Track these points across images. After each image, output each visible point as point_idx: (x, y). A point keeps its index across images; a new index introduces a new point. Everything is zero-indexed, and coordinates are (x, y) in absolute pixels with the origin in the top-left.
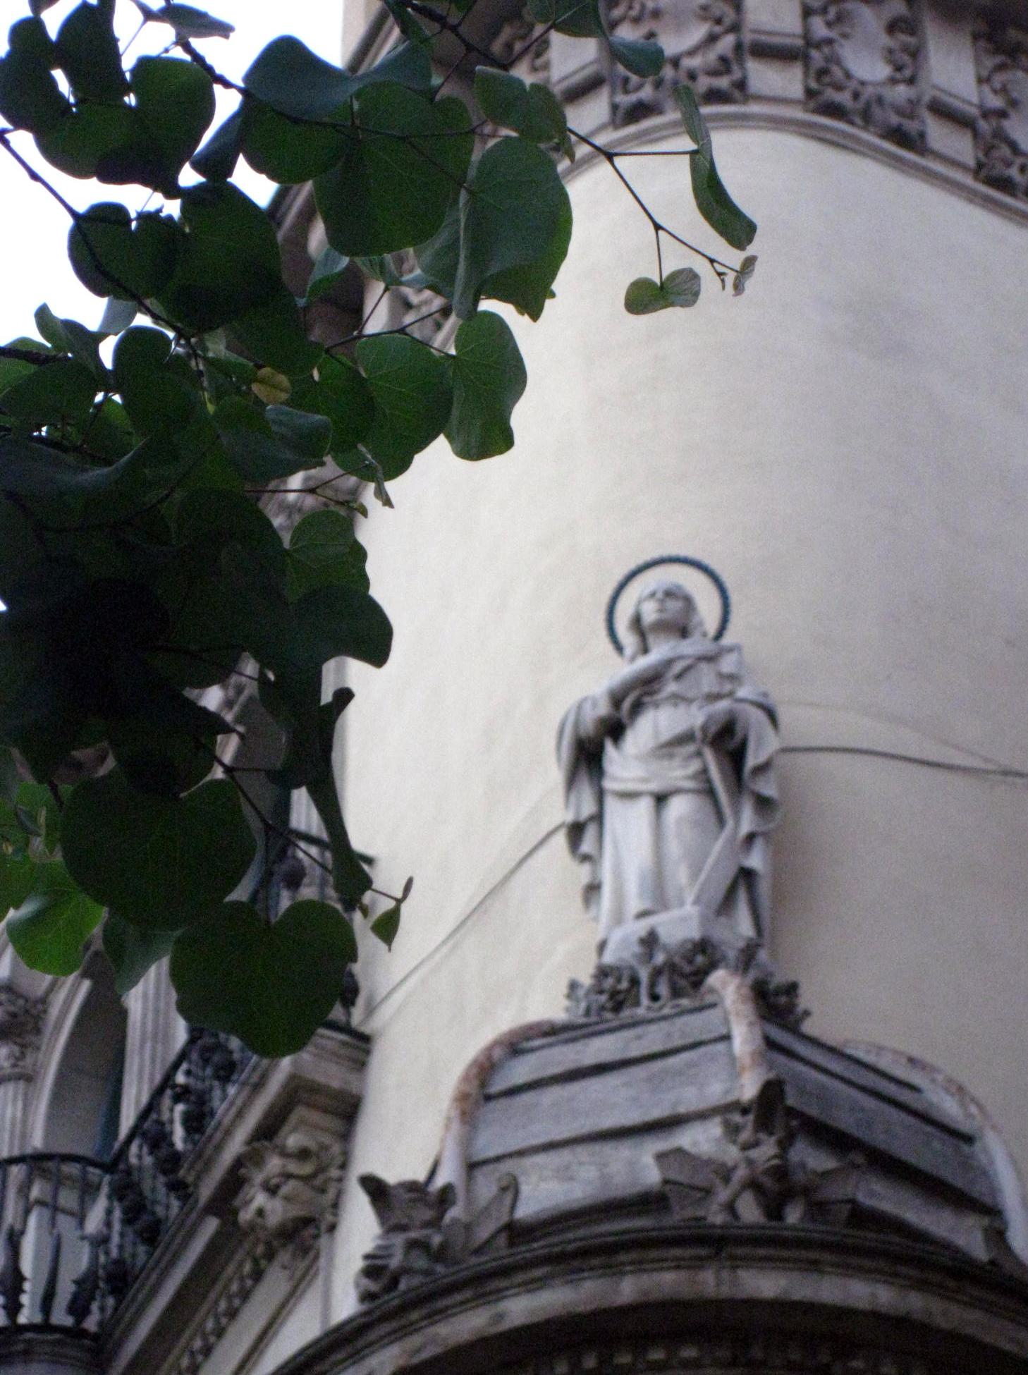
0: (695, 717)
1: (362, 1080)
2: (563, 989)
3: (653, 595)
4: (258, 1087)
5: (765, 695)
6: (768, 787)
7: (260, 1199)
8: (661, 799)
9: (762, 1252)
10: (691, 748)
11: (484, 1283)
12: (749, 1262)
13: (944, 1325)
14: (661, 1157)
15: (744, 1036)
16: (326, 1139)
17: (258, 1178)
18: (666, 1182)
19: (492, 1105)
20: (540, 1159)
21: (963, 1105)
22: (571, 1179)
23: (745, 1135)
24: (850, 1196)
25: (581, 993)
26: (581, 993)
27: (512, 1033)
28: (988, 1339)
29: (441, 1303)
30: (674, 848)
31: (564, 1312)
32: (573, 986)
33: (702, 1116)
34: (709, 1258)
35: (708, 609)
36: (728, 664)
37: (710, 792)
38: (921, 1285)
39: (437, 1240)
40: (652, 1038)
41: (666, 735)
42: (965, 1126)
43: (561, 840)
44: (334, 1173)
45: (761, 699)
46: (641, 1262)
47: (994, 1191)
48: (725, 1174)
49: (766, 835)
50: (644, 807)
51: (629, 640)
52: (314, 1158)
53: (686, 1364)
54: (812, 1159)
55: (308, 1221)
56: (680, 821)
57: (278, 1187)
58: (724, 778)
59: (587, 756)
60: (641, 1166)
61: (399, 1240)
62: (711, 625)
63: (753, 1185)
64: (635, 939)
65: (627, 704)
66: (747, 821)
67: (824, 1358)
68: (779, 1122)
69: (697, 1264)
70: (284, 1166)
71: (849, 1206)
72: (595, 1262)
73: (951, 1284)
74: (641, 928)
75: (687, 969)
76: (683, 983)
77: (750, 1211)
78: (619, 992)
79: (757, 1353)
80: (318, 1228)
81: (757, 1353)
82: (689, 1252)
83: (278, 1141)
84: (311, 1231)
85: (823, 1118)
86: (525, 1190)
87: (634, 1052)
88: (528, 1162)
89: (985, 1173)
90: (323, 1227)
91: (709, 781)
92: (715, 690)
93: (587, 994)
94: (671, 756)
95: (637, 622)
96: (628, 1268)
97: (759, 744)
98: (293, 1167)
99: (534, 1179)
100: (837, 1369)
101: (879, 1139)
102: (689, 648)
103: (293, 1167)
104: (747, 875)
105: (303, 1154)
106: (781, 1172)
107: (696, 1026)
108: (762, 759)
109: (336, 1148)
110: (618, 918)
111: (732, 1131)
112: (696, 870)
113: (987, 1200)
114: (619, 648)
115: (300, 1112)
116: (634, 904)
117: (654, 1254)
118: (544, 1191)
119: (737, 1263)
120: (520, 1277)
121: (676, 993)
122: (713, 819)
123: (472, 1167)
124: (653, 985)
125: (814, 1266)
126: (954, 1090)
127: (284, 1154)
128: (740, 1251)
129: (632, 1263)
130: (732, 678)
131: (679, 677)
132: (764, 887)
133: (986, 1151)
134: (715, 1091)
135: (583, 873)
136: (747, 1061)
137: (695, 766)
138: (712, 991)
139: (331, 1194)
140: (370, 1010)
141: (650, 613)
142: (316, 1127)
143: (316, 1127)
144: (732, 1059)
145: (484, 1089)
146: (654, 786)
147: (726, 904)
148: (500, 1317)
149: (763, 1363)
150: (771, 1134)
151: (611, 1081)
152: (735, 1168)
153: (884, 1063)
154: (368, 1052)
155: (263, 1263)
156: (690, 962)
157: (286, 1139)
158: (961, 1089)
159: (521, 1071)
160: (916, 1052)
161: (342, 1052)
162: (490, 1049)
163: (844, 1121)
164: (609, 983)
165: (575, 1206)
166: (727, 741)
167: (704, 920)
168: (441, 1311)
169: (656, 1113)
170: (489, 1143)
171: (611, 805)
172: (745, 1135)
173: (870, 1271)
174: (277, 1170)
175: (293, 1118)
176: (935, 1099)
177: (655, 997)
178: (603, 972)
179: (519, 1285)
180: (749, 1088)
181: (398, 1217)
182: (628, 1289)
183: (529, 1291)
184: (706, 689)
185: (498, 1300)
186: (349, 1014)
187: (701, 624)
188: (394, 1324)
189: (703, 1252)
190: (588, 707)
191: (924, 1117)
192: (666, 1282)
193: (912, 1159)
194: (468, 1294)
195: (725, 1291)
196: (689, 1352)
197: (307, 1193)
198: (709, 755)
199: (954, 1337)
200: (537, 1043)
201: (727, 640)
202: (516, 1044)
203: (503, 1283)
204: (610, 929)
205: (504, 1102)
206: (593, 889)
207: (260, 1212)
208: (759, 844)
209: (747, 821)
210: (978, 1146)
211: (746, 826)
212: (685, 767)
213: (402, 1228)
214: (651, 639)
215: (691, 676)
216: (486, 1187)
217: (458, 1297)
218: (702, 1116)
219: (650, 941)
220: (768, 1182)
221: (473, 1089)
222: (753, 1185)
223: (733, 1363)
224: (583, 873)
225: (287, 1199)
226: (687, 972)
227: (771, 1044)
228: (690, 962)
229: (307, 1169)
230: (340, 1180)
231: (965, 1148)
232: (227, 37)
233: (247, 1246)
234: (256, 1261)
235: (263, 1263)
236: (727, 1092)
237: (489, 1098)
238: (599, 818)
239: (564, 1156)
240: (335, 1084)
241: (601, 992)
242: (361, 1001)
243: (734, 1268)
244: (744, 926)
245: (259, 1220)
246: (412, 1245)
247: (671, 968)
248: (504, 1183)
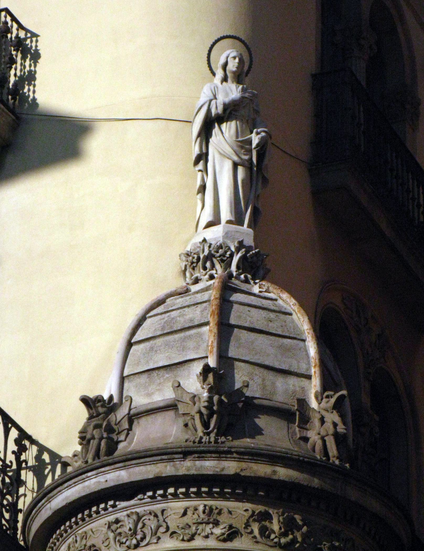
65: (228, 112)
75: (250, 260)
148: (274, 472)
169: (284, 367)
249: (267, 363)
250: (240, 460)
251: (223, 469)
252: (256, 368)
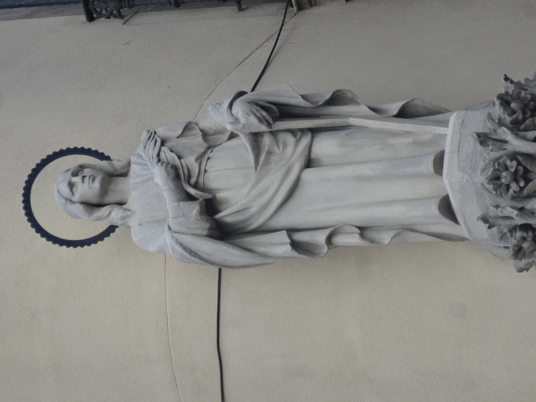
3: (71, 185)
10: (267, 141)
37: (314, 131)
131: (180, 158)
238: (291, 231)
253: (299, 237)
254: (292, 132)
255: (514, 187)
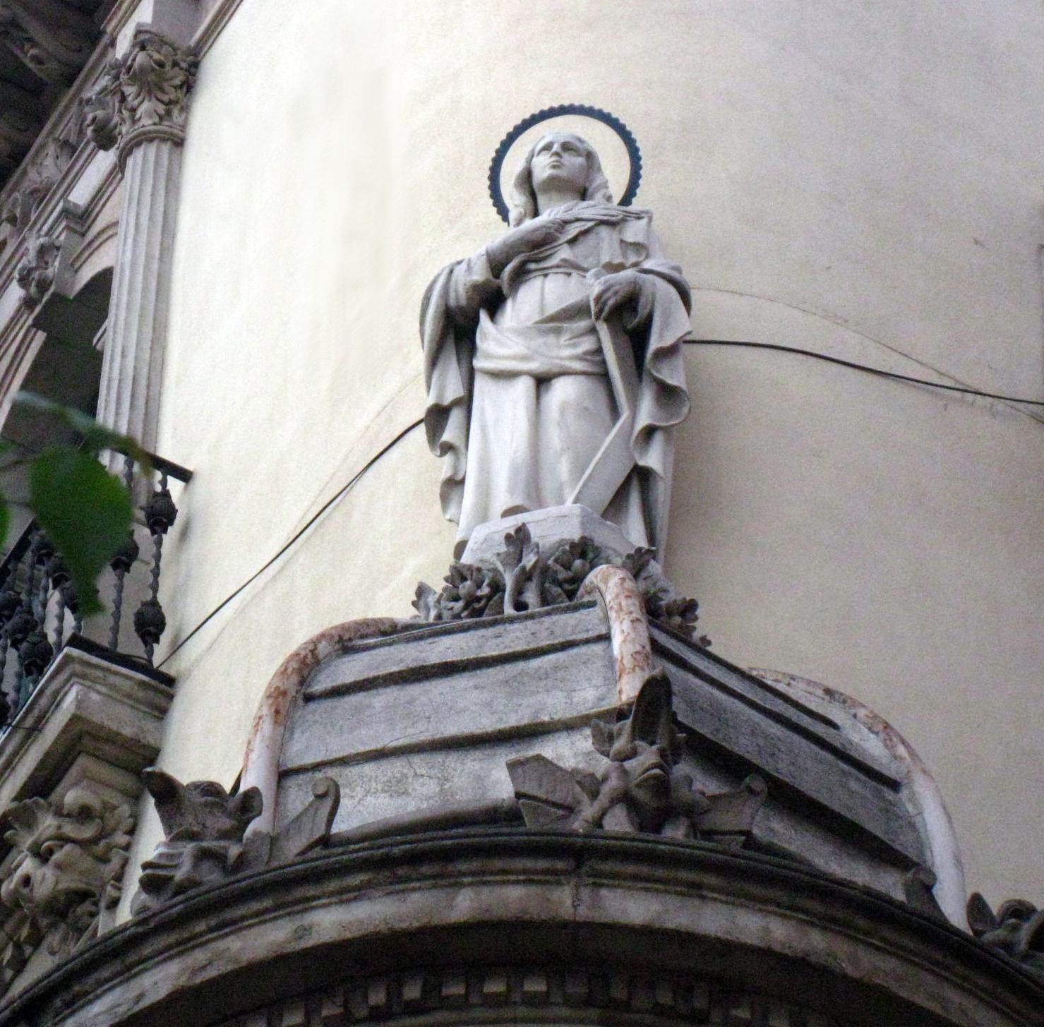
0: (589, 287)
1: (162, 731)
2: (415, 588)
3: (547, 147)
4: (34, 731)
5: (678, 269)
6: (673, 375)
7: (28, 865)
8: (542, 381)
9: (631, 869)
10: (583, 324)
11: (290, 887)
12: (616, 879)
13: (850, 970)
14: (512, 766)
15: (625, 634)
16: (112, 797)
17: (27, 841)
18: (519, 795)
19: (312, 706)
20: (369, 768)
21: (888, 745)
22: (405, 793)
23: (620, 744)
24: (745, 828)
25: (431, 600)
26: (431, 600)
27: (343, 627)
28: (904, 994)
29: (298, 893)
30: (554, 437)
31: (383, 928)
32: (422, 591)
33: (570, 726)
34: (565, 873)
35: (614, 171)
36: (633, 232)
38: (827, 924)
39: (234, 851)
40: (515, 637)
41: (552, 309)
42: (891, 771)
43: (421, 433)
44: (121, 839)
45: (675, 274)
46: (483, 873)
47: (921, 844)
48: (592, 786)
49: (666, 430)
50: (524, 387)
51: (514, 199)
52: (98, 820)
53: (532, 1000)
54: (699, 783)
55: (83, 896)
56: (563, 409)
57: (51, 852)
58: (621, 360)
59: (456, 330)
60: (494, 780)
61: (188, 848)
62: (618, 191)
63: (625, 798)
64: (500, 538)
66: (647, 413)
67: (700, 1002)
68: (662, 729)
69: (553, 878)
70: (59, 827)
71: (743, 838)
72: (425, 869)
73: (861, 922)
74: (511, 524)
75: (563, 574)
76: (556, 590)
77: (618, 823)
78: (478, 599)
79: (618, 992)
80: (96, 904)
81: (618, 992)
82: (542, 864)
83: (54, 797)
84: (87, 906)
85: (718, 738)
86: (345, 803)
87: (492, 651)
88: (353, 772)
89: (912, 826)
90: (103, 904)
91: (604, 362)
92: (618, 260)
93: (438, 601)
94: (558, 332)
95: (526, 178)
96: (467, 880)
97: (665, 325)
98: (69, 829)
99: (359, 791)
100: (716, 1017)
101: (782, 769)
102: (588, 210)
103: (69, 829)
104: (642, 476)
105: (84, 814)
106: (661, 785)
107: (566, 624)
108: (668, 342)
109: (125, 809)
110: (482, 515)
111: (604, 740)
112: (578, 467)
113: (912, 854)
114: (503, 212)
115: (82, 762)
116: (502, 500)
117: (498, 864)
118: (367, 805)
119: (599, 880)
120: (333, 885)
121: (545, 600)
122: (604, 410)
123: (283, 775)
124: (519, 591)
125: (695, 890)
126: (880, 727)
127: (59, 812)
128: (607, 867)
129: (473, 874)
130: (638, 247)
131: (572, 242)
132: (662, 491)
133: (913, 799)
134: (588, 694)
135: (444, 467)
136: (628, 663)
137: (587, 344)
138: (594, 589)
139: (116, 862)
140: (176, 647)
141: (543, 168)
142: (103, 783)
143: (103, 783)
144: (610, 662)
145: (304, 686)
146: (534, 366)
147: (615, 506)
148: (306, 930)
149: (626, 1006)
150: (652, 743)
151: (461, 682)
152: (605, 778)
153: (796, 692)
154: (171, 697)
155: (28, 950)
156: (567, 567)
157: (63, 796)
158: (887, 726)
159: (351, 669)
160: (831, 685)
161: (141, 694)
162: (315, 642)
163: (743, 746)
164: (465, 588)
165: (407, 819)
166: (627, 317)
167: (585, 520)
168: (234, 922)
169: (513, 720)
170: (304, 750)
171: (480, 383)
172: (620, 744)
173: (765, 901)
174: (51, 832)
175: (74, 772)
176: (855, 738)
177: (520, 606)
178: (459, 575)
179: (331, 894)
180: (629, 689)
181: (190, 823)
182: (464, 904)
183: (342, 902)
184: (605, 258)
185: (305, 910)
186: (150, 653)
187: (605, 185)
188: (172, 938)
189: (560, 865)
190: (460, 271)
191: (842, 755)
192: (511, 898)
193: (823, 798)
194: (267, 903)
195: (584, 913)
196: (536, 986)
197: (87, 862)
198: (603, 330)
199: (864, 989)
200: (371, 641)
201: (636, 205)
202: (347, 641)
203: (311, 891)
204: (471, 529)
205: (327, 704)
206: (454, 484)
207: (27, 881)
208: (658, 439)
209: (647, 413)
210: (904, 793)
211: (645, 417)
212: (574, 346)
213: (192, 836)
214: (541, 200)
215: (590, 240)
216: (299, 797)
217: (256, 906)
218: (570, 726)
219: (519, 539)
220: (642, 795)
221: (291, 683)
222: (625, 798)
223: (588, 1002)
224: (444, 467)
225: (59, 867)
226: (560, 578)
227: (658, 649)
228: (567, 567)
229: (88, 832)
230: (127, 847)
231: (889, 794)
232: (142, 602)
233: (8, 927)
234: (18, 947)
235: (28, 950)
236: (601, 699)
237: (309, 698)
238: (466, 402)
239: (395, 767)
240: (127, 731)
241: (456, 599)
242: (165, 638)
243: (597, 886)
244: (636, 535)
245: (25, 891)
246: (204, 855)
247: (542, 571)
248: (321, 790)
249: (452, 729)
250: (183, 947)
251: (140, 997)
252: (417, 759)
253: (456, 417)
254: (599, 351)
255: (459, 605)
